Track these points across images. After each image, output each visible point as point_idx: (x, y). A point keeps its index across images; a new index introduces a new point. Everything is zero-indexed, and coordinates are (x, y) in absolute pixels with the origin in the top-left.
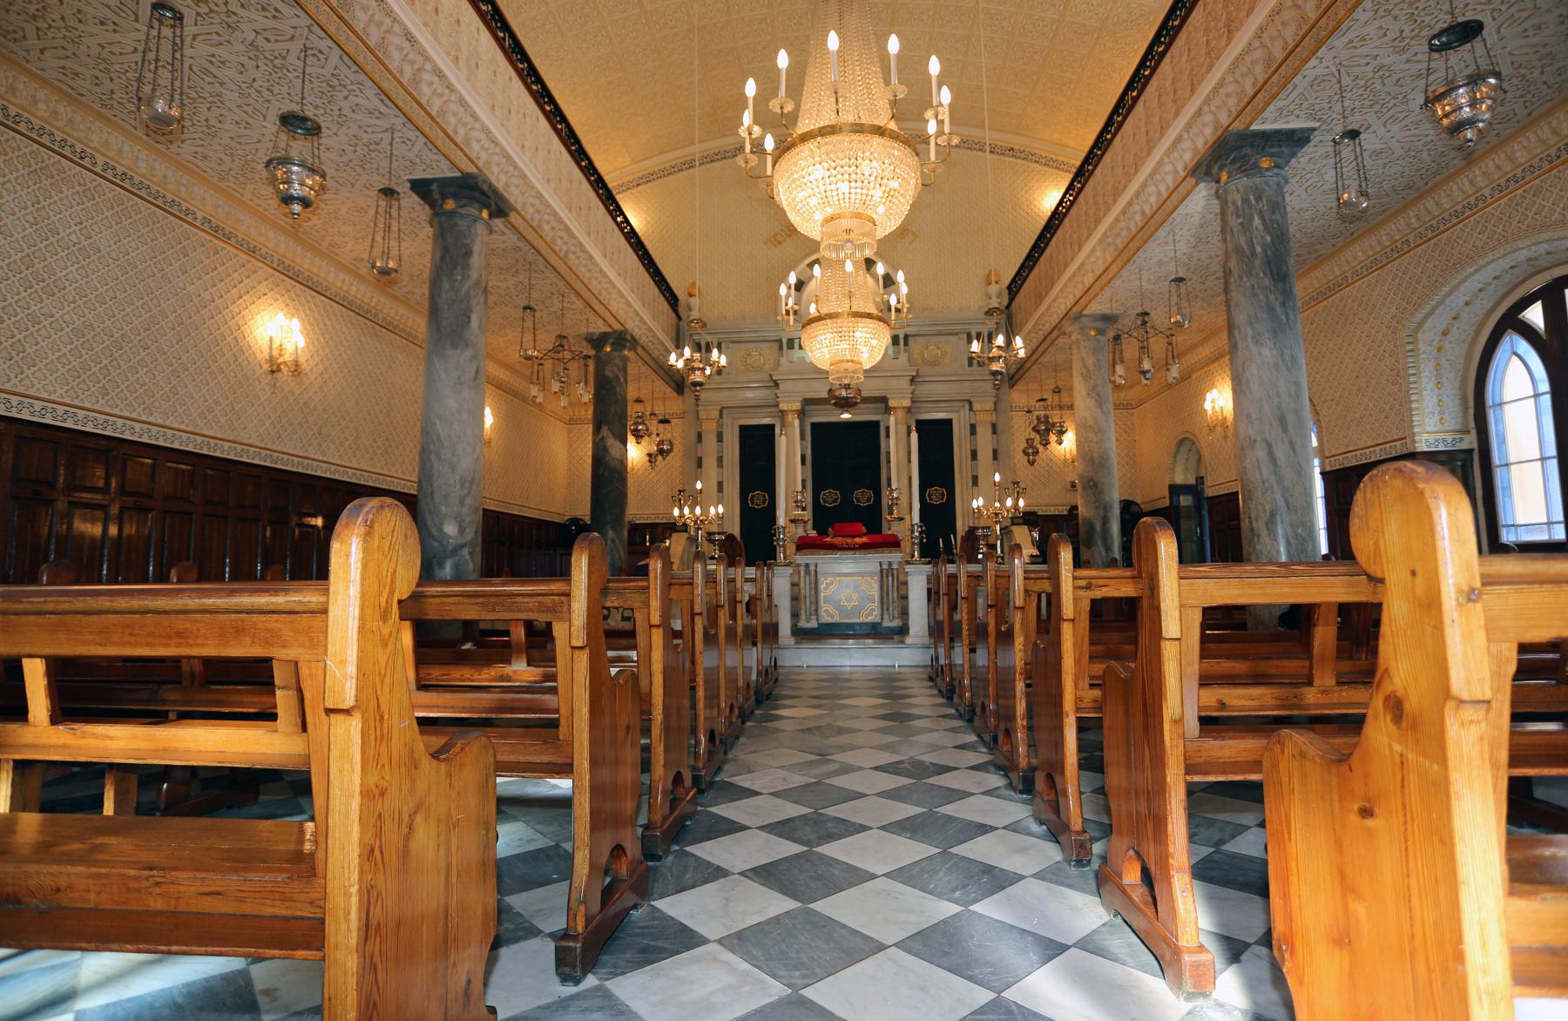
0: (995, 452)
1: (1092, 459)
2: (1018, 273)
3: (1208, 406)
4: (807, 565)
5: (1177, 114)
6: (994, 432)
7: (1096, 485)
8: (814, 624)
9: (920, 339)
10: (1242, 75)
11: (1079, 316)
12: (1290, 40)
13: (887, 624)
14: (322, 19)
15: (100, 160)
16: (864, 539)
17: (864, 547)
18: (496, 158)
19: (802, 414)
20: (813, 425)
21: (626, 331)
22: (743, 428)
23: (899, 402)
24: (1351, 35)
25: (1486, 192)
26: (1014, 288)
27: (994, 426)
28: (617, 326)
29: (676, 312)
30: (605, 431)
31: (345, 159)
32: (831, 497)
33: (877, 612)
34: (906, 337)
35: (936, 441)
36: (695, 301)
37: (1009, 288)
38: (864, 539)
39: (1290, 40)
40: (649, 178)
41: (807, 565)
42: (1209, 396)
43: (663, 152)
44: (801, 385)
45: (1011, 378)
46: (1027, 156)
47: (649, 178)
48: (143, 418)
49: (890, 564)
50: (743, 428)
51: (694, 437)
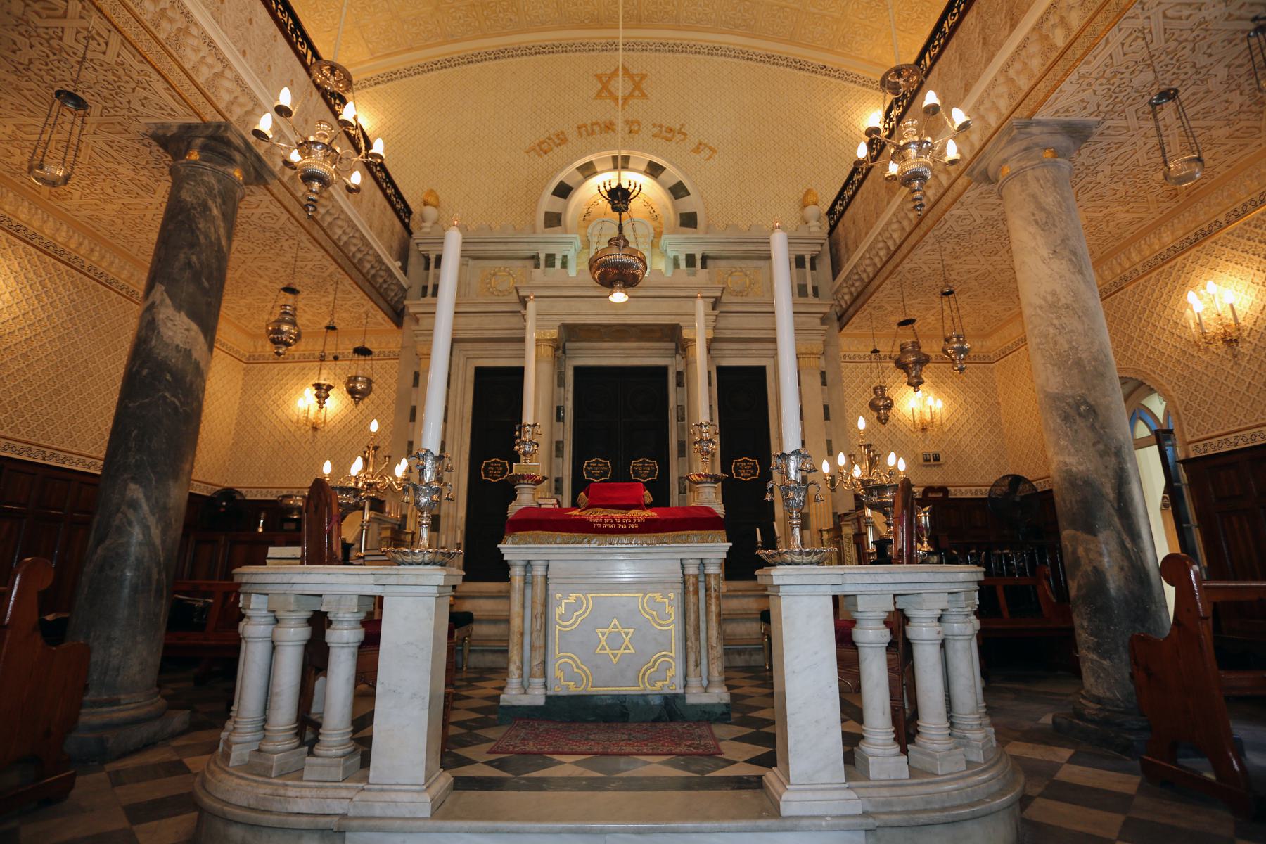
0: (826, 408)
1: (1078, 363)
2: (840, 195)
3: (1190, 317)
4: (528, 565)
5: (989, 60)
6: (824, 383)
7: (1092, 410)
8: (536, 697)
9: (723, 263)
10: (1018, 73)
11: (1028, 123)
12: (1036, 71)
13: (696, 697)
14: (145, 37)
15: (87, 263)
16: (649, 513)
17: (647, 527)
18: (354, 241)
19: (560, 348)
20: (577, 370)
21: (227, 125)
22: (479, 372)
23: (699, 333)
24: (926, 248)
25: (1139, 267)
26: (835, 214)
27: (823, 374)
28: (210, 116)
29: (407, 227)
30: (160, 289)
31: (277, 276)
32: (597, 466)
33: (676, 670)
34: (705, 259)
35: (744, 395)
36: (430, 212)
37: (831, 212)
38: (649, 513)
39: (1036, 71)
40: (391, 77)
41: (528, 565)
42: (1191, 296)
43: (410, 49)
44: (561, 306)
45: (839, 319)
46: (843, 75)
47: (391, 77)
48: (41, 442)
49: (702, 564)
50: (479, 372)
51: (410, 379)
